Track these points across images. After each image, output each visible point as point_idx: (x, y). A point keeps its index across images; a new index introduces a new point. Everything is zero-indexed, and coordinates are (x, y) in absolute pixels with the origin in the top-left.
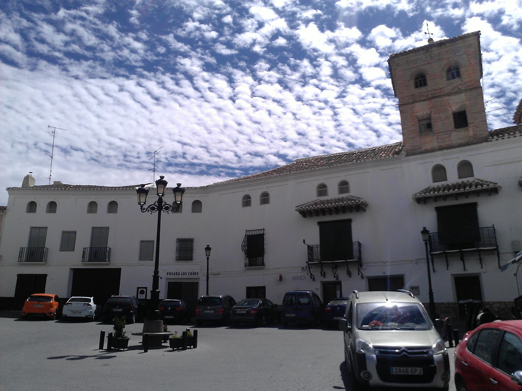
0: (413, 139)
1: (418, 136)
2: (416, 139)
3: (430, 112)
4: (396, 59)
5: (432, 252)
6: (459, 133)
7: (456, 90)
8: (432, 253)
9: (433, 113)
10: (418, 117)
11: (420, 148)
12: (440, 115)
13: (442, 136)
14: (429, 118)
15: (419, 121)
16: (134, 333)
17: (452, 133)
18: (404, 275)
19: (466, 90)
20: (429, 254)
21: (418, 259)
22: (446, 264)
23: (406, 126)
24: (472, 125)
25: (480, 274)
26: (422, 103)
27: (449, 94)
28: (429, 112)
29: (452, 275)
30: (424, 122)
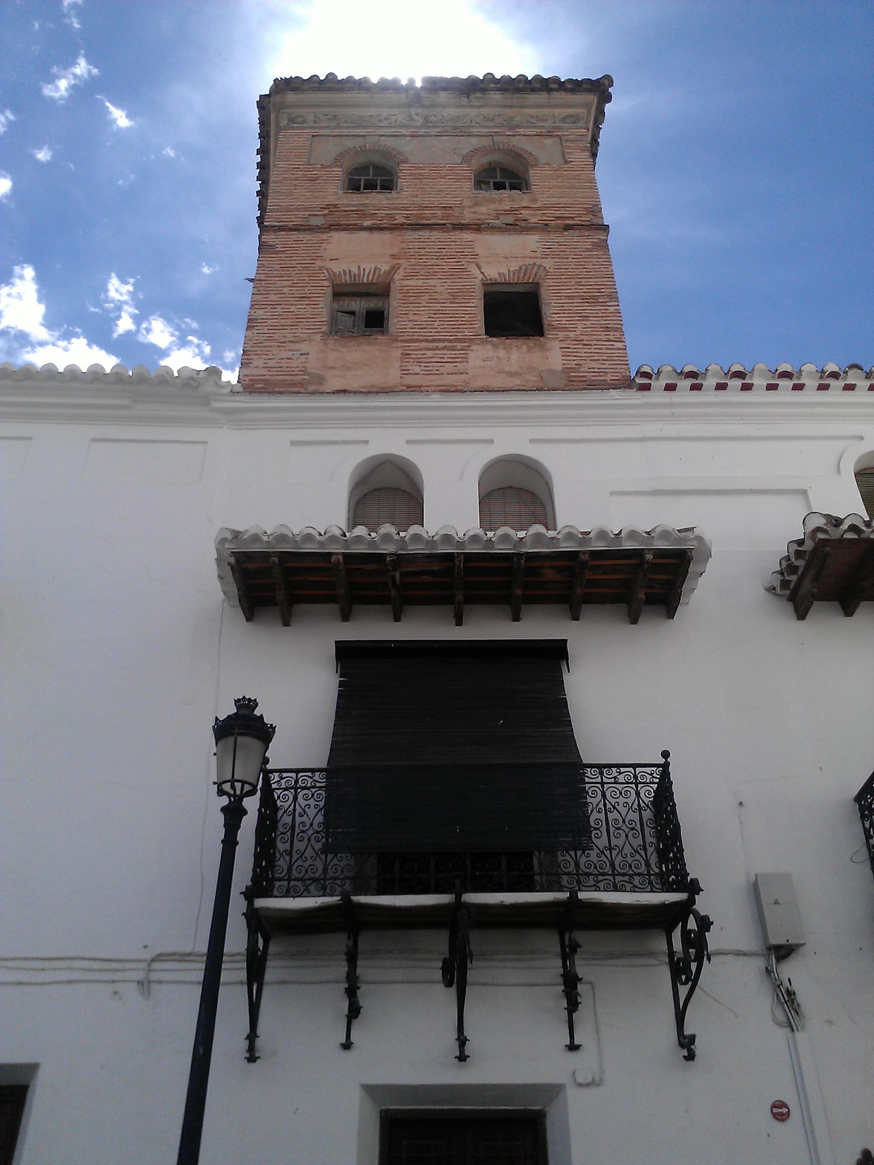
0: (293, 346)
1: (318, 337)
2: (304, 347)
3: (393, 268)
4: (291, 97)
5: (267, 893)
6: (502, 353)
7: (510, 220)
8: (261, 903)
9: (401, 271)
10: (332, 277)
11: (321, 380)
12: (431, 282)
13: (430, 353)
14: (382, 291)
15: (339, 293)
16: (576, 1074)
17: (474, 347)
18: (32, 1069)
19: (544, 228)
20: (237, 905)
21: (159, 958)
22: (344, 1005)
23: (272, 297)
24: (561, 335)
25: (553, 1091)
26: (364, 235)
27: (478, 228)
28: (385, 268)
29: (370, 1090)
30: (359, 305)
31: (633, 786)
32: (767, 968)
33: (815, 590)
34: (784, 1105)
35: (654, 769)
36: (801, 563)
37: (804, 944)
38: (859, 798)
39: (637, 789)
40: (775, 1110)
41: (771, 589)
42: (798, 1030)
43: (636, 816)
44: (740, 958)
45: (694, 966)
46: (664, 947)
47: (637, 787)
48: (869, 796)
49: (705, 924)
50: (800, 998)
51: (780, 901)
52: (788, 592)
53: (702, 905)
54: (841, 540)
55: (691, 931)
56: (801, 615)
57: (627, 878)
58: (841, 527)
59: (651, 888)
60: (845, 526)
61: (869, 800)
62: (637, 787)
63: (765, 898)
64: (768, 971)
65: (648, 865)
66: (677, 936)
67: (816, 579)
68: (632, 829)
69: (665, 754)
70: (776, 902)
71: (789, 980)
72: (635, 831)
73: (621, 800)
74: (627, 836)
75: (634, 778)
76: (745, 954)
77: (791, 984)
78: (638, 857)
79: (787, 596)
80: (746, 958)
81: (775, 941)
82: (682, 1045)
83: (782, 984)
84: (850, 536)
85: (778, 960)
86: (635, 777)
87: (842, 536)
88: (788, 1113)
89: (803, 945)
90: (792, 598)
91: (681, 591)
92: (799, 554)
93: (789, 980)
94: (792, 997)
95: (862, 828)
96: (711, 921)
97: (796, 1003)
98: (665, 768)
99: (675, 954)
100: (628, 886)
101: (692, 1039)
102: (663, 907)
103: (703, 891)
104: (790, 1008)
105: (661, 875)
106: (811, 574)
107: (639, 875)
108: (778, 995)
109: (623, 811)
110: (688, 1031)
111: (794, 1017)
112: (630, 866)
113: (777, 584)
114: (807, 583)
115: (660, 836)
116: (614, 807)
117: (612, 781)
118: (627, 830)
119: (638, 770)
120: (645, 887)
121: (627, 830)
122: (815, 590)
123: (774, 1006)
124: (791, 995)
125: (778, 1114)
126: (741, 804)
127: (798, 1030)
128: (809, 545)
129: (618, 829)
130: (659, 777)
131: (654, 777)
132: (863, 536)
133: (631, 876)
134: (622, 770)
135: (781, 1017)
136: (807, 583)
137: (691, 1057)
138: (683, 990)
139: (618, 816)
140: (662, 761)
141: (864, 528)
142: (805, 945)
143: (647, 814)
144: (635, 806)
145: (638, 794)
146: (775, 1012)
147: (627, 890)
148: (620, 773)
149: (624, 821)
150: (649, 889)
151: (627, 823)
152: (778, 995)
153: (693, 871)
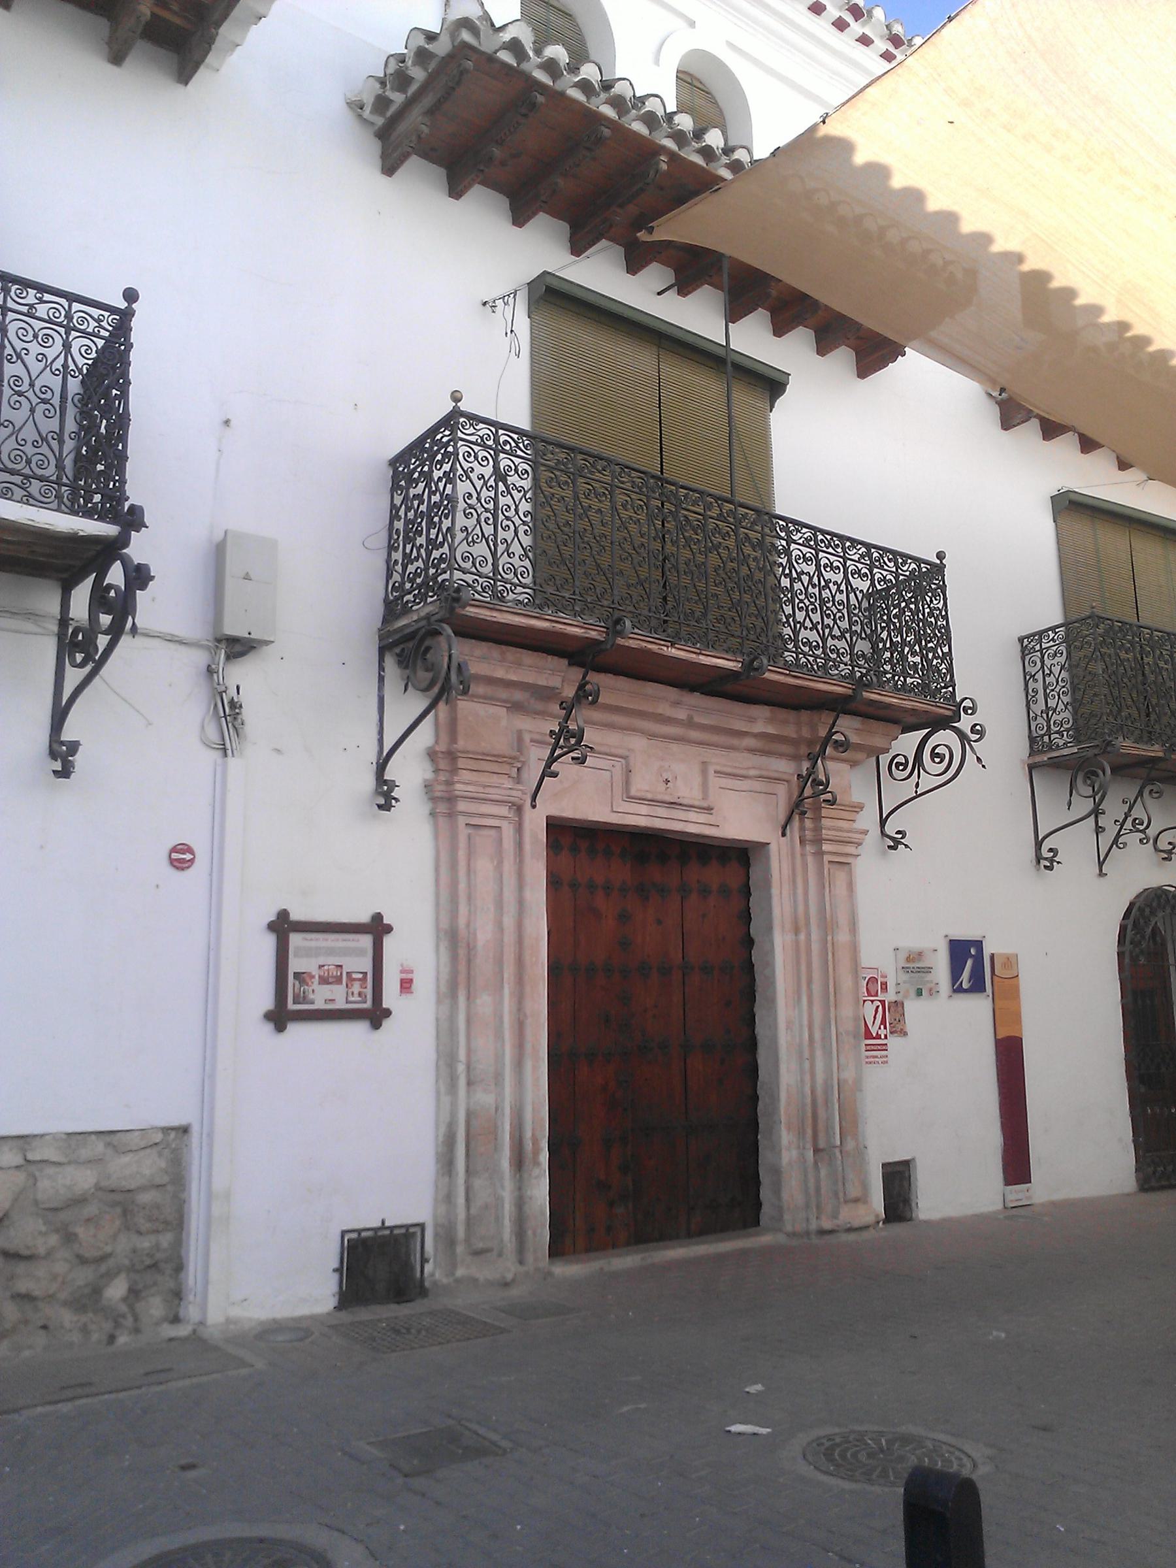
31: (62, 330)
32: (209, 666)
33: (425, 129)
34: (190, 850)
35: (106, 314)
36: (418, 74)
37: (273, 642)
38: (394, 462)
39: (67, 338)
40: (175, 856)
41: (356, 106)
42: (233, 756)
43: (56, 383)
44: (171, 645)
45: (102, 641)
46: (55, 609)
47: (68, 333)
48: (413, 460)
49: (139, 577)
50: (247, 713)
51: (252, 576)
52: (380, 121)
53: (139, 549)
54: (491, 59)
55: (110, 587)
56: (389, 168)
57: (17, 479)
58: (501, 35)
59: (59, 506)
60: (506, 36)
61: (412, 467)
62: (68, 333)
63: (233, 568)
64: (210, 671)
65: (60, 466)
66: (81, 595)
67: (431, 112)
68: (44, 401)
69: (131, 295)
70: (247, 577)
71: (238, 688)
72: (48, 406)
73: (35, 348)
74: (32, 410)
75: (65, 317)
76: (181, 642)
77: (238, 693)
78: (45, 449)
79: (377, 128)
80: (182, 648)
81: (230, 630)
82: (53, 755)
83: (225, 692)
84: (506, 57)
85: (229, 657)
86: (69, 317)
87: (496, 52)
88: (192, 861)
89: (267, 643)
90: (383, 134)
91: (217, 34)
92: (422, 56)
93: (238, 688)
94: (237, 711)
95: (390, 502)
96: (152, 574)
97: (240, 721)
98: (124, 318)
99: (71, 622)
100: (19, 493)
101: (74, 747)
102: (74, 539)
103: (147, 527)
104: (230, 725)
105: (74, 489)
106: (428, 101)
107: (41, 479)
108: (216, 705)
109: (35, 367)
110: (67, 735)
111: (232, 738)
112: (29, 462)
113: (369, 100)
114: (416, 116)
115: (87, 428)
116: (19, 356)
117: (25, 309)
118: (35, 401)
119: (76, 306)
120: (48, 500)
121: (35, 401)
122: (425, 129)
123: (207, 721)
124: (236, 708)
125: (179, 860)
126: (227, 422)
127: (233, 756)
128: (442, 48)
129: (20, 394)
130: (111, 328)
131: (101, 327)
132: (525, 66)
133: (27, 477)
134: (47, 297)
135: (212, 734)
136: (416, 116)
137: (65, 772)
138: (73, 676)
139: (22, 372)
140: (123, 305)
141: (531, 54)
142: (273, 644)
143: (74, 385)
144: (58, 364)
145: (67, 346)
146: (205, 726)
147: (14, 498)
148: (41, 301)
149: (32, 385)
150: (54, 505)
151: (37, 389)
152: (216, 705)
153: (136, 493)
